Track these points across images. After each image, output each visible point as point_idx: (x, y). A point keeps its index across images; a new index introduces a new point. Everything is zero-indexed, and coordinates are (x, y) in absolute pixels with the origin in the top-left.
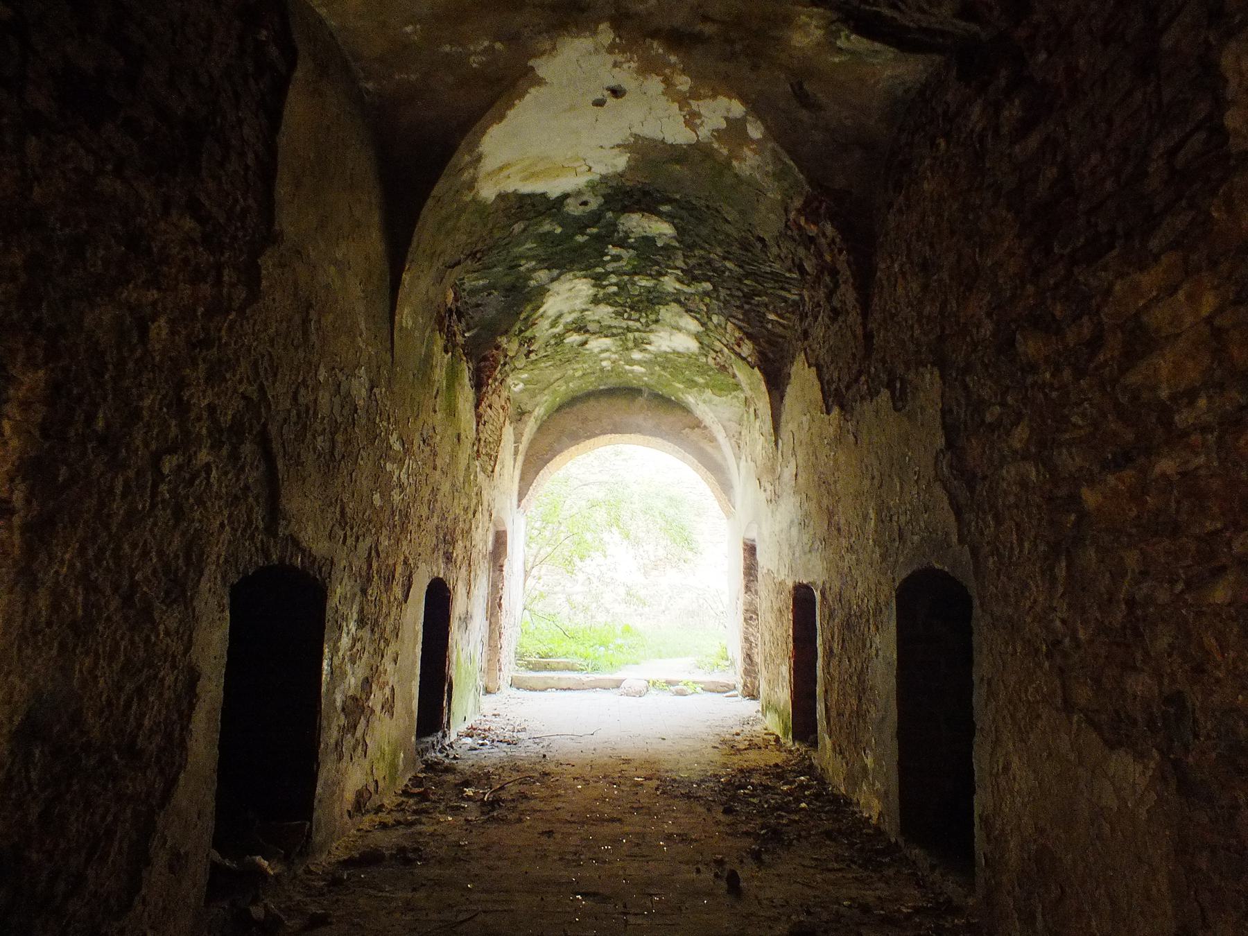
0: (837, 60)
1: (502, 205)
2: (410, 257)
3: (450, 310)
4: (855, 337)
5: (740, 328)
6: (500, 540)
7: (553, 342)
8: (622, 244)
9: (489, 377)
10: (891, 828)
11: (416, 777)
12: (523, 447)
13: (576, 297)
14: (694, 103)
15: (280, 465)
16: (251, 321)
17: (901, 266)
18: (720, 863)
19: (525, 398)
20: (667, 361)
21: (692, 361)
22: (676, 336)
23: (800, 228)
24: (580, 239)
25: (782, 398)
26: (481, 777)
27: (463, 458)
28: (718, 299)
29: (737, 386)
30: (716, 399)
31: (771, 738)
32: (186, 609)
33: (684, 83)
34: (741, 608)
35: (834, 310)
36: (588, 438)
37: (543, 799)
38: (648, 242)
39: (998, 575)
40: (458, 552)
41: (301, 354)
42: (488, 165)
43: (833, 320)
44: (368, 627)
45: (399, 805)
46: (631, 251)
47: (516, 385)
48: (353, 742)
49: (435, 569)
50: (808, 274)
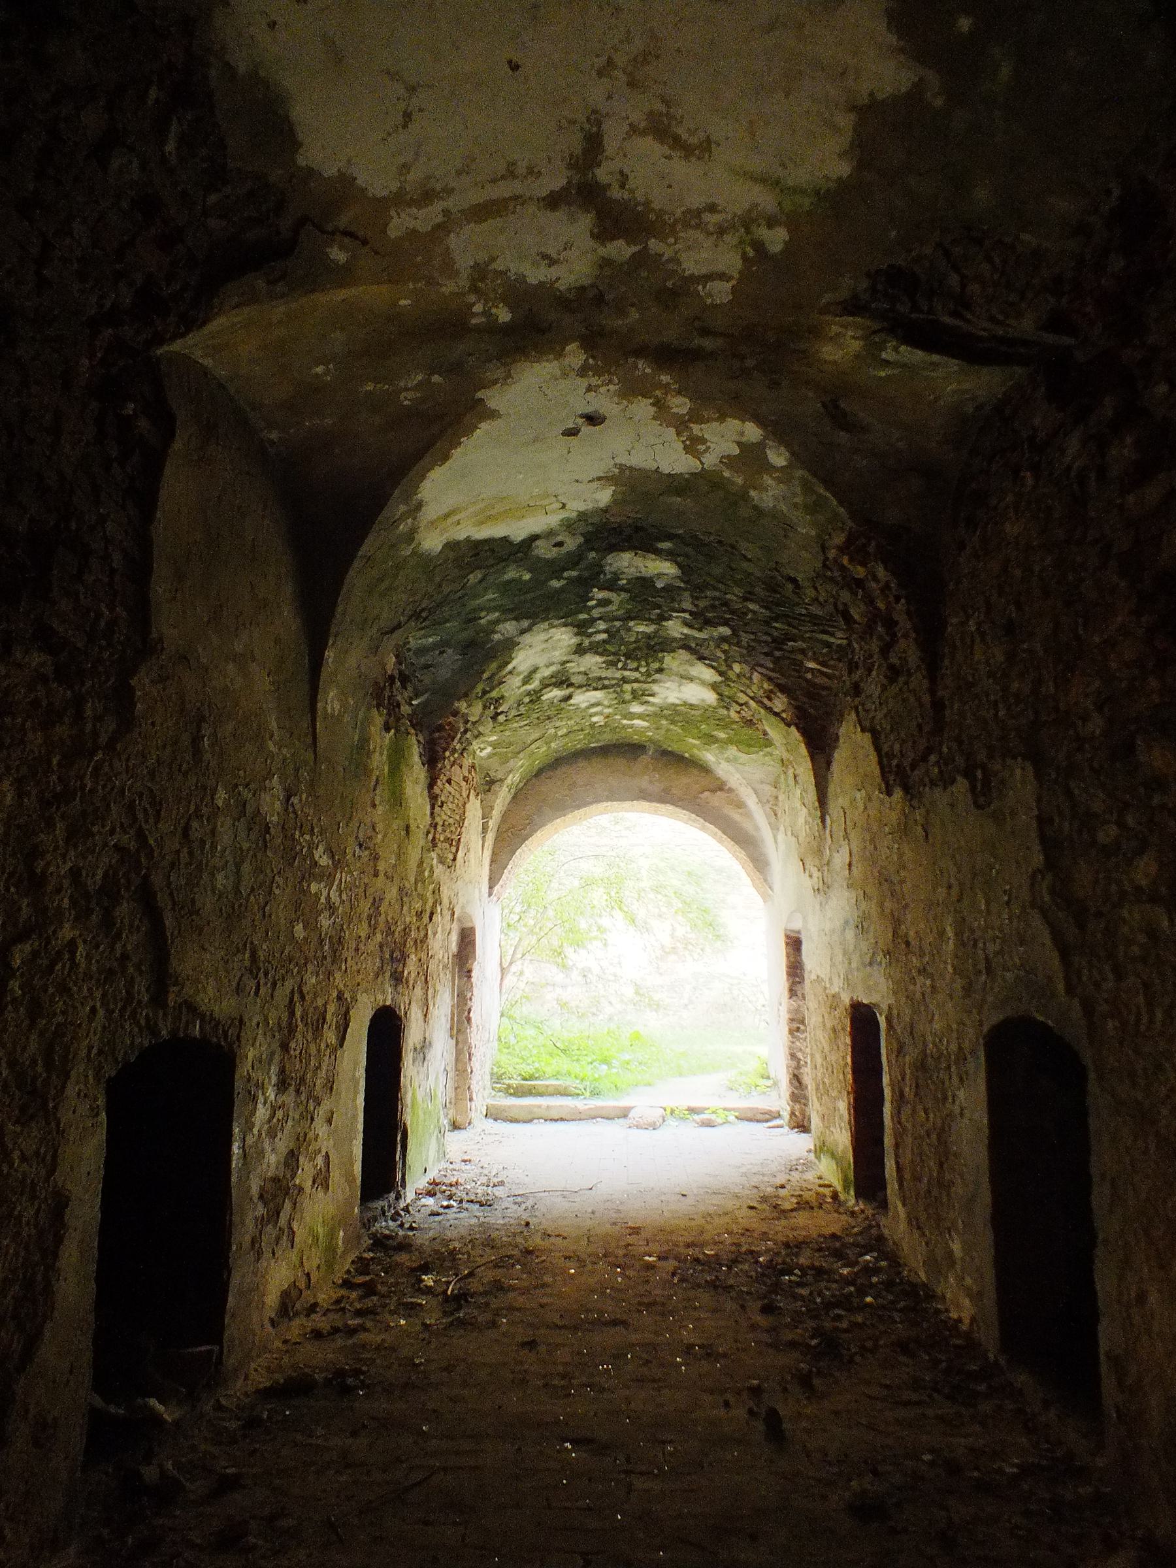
0: (883, 374)
1: (452, 555)
2: (333, 630)
3: (392, 679)
4: (921, 705)
5: (770, 679)
6: (467, 939)
7: (527, 700)
8: (611, 586)
9: (445, 750)
10: (989, 1338)
11: (360, 1259)
12: (493, 823)
13: (554, 649)
14: (696, 428)
15: (169, 922)
16: (124, 757)
17: (979, 624)
18: (756, 1391)
19: (494, 763)
20: (677, 714)
21: (708, 714)
22: (687, 686)
23: (843, 568)
24: (556, 584)
25: (829, 763)
26: (444, 1257)
27: (414, 855)
28: (738, 644)
29: (769, 743)
30: (743, 757)
31: (827, 1191)
32: (48, 1123)
33: (680, 405)
34: (785, 1016)
35: (891, 667)
36: (578, 807)
37: (524, 1292)
38: (644, 584)
39: (1121, 1043)
40: (411, 968)
41: (192, 779)
42: (430, 512)
43: (892, 680)
44: (292, 1088)
45: (338, 1301)
46: (624, 595)
47: (482, 750)
48: (274, 1234)
49: (380, 997)
50: (855, 622)
